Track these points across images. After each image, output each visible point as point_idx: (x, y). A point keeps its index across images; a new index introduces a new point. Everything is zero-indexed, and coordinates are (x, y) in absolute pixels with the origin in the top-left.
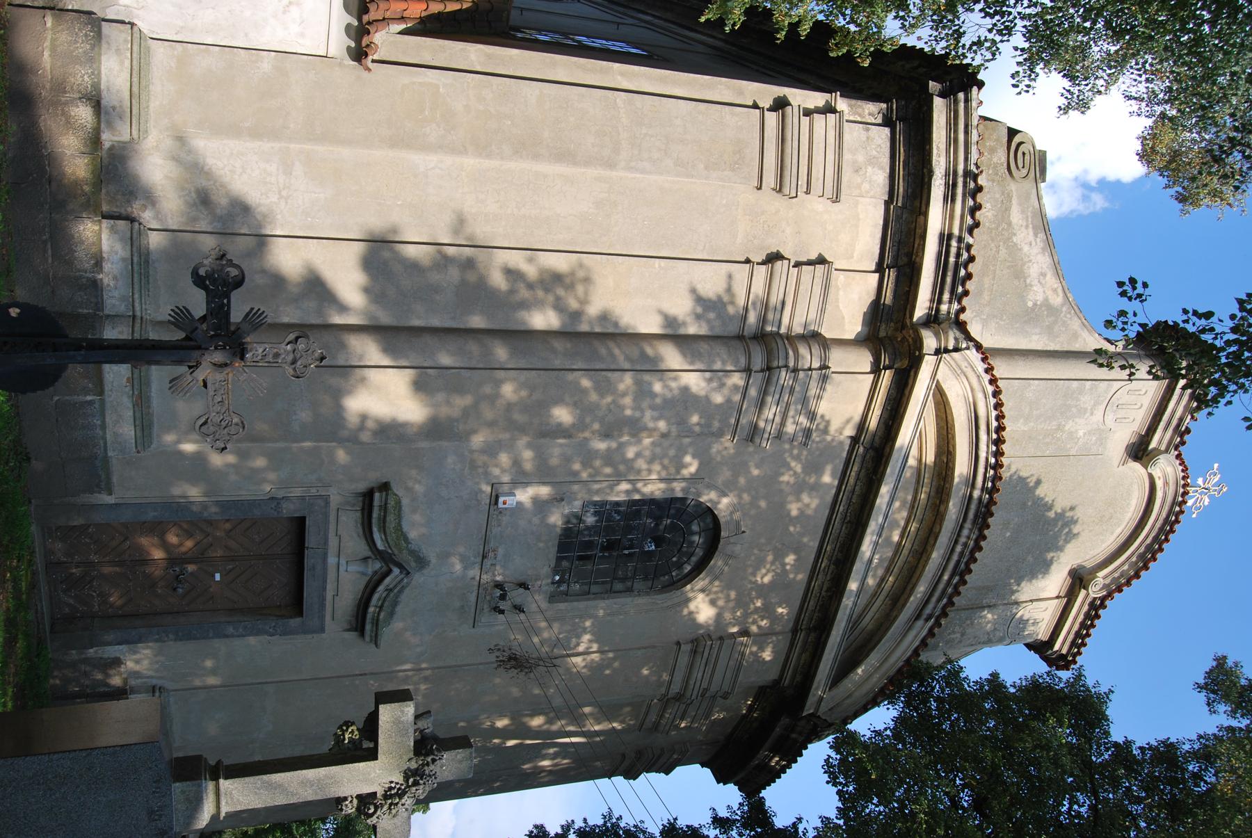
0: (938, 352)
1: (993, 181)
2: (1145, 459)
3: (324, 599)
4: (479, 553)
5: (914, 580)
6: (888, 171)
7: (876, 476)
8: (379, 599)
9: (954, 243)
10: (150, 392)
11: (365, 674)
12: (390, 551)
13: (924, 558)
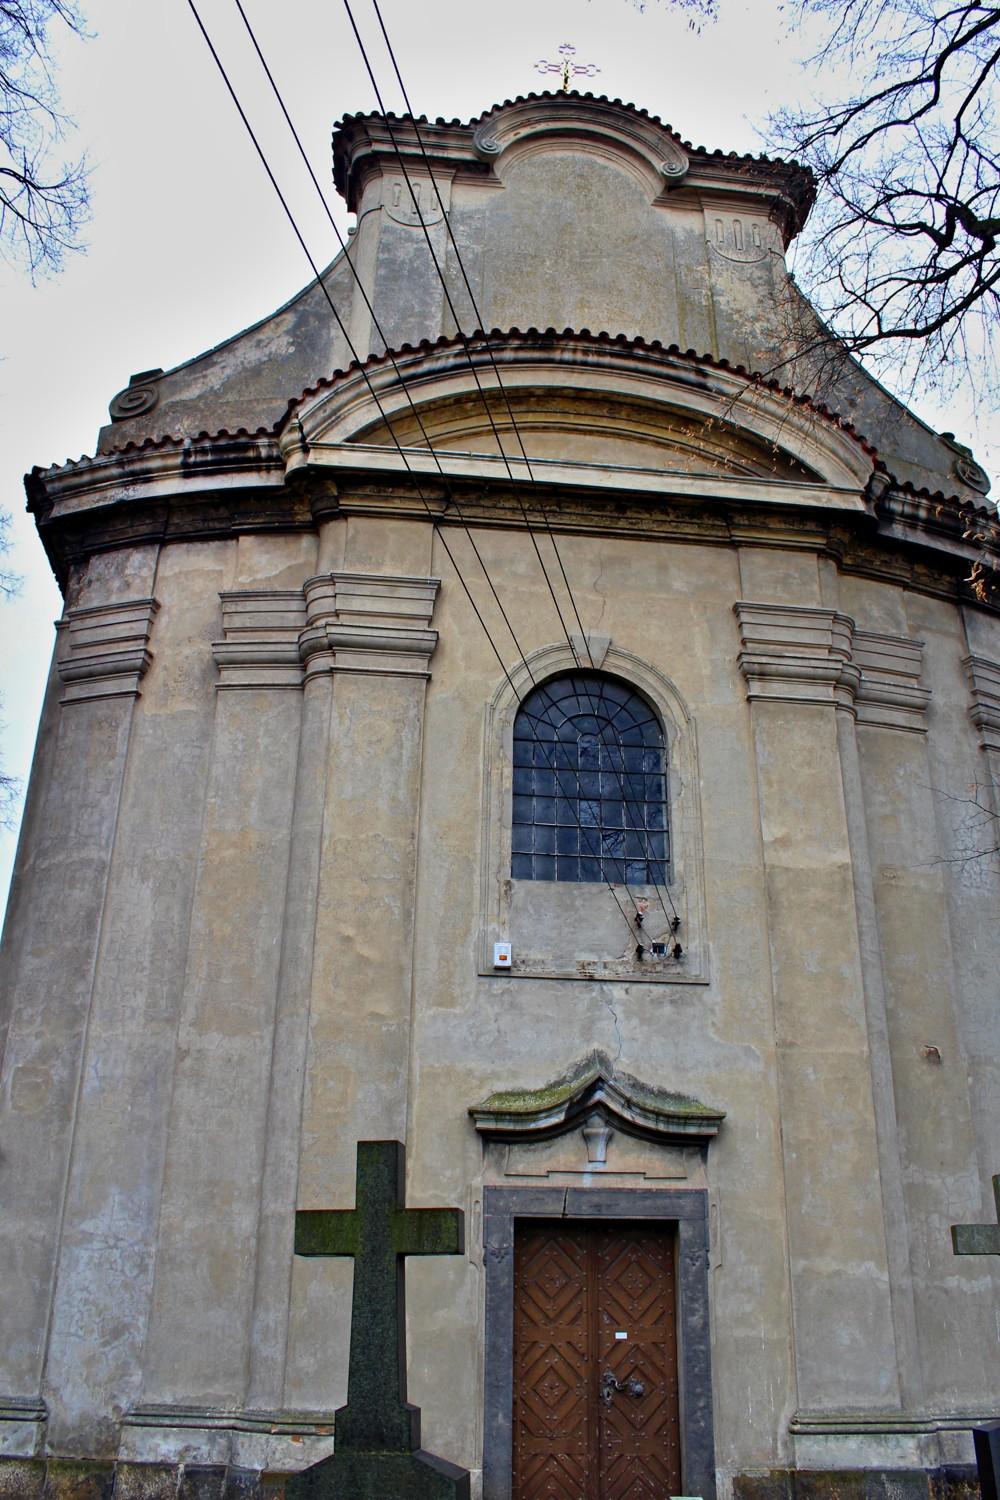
1: (153, 428)
3: (648, 1191)
4: (587, 986)
5: (650, 404)
8: (646, 1117)
10: (318, 1412)
12: (567, 1105)
13: (615, 398)
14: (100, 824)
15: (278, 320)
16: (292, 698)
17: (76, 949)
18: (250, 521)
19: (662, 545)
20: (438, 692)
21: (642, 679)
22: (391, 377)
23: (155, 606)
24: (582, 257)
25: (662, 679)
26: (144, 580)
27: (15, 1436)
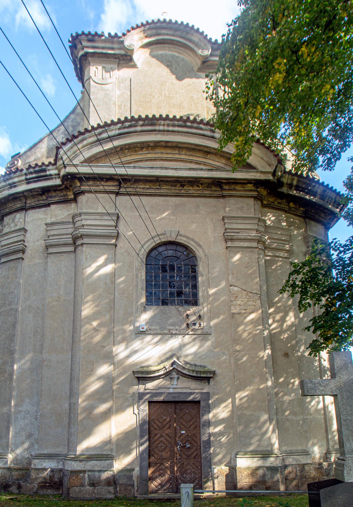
5: (193, 147)
6: (16, 214)
8: (189, 372)
9: (28, 177)
13: (180, 145)
14: (14, 298)
15: (58, 129)
16: (72, 255)
17: (10, 334)
18: (53, 199)
19: (197, 199)
20: (119, 250)
21: (189, 243)
22: (94, 139)
23: (25, 230)
24: (169, 94)
25: (196, 243)
26: (21, 223)
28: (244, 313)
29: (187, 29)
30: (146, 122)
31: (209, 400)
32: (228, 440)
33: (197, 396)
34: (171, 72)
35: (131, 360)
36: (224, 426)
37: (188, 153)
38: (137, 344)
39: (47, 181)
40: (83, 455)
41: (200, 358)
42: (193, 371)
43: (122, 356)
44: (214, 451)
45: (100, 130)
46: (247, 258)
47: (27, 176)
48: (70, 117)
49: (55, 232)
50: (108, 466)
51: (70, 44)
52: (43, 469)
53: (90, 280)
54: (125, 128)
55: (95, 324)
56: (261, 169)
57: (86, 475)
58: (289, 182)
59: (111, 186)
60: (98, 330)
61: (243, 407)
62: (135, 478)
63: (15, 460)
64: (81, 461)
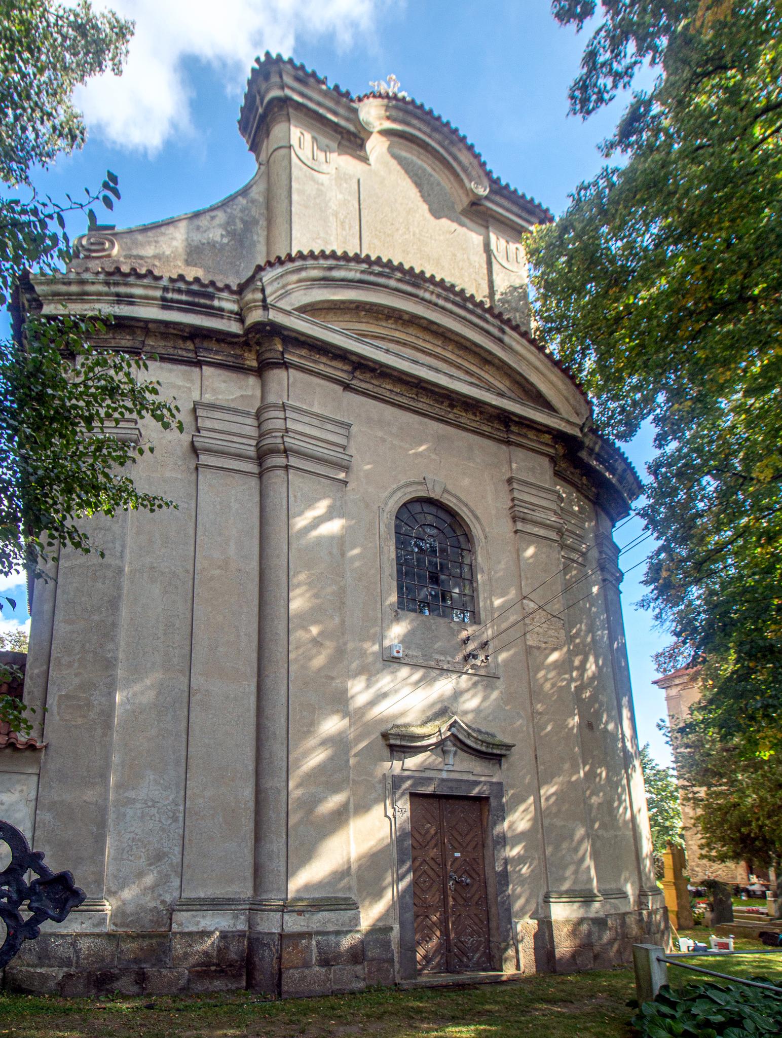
0: (265, 307)
2: (362, 135)
5: (468, 344)
7: (376, 370)
8: (476, 743)
9: (170, 295)
11: (536, 755)
13: (449, 335)
14: (113, 542)
15: (213, 214)
25: (472, 511)
27: (90, 921)
28: (545, 649)
29: (454, 137)
30: (407, 278)
31: (502, 796)
32: (532, 871)
33: (485, 788)
34: (422, 196)
35: (377, 711)
36: (524, 847)
37: (457, 352)
38: (385, 682)
39: (211, 318)
40: (301, 899)
41: (485, 719)
42: (483, 742)
43: (361, 700)
44: (514, 890)
45: (331, 262)
46: (544, 556)
47: (168, 292)
48: (236, 201)
49: (217, 425)
50: (350, 921)
51: (257, 66)
52: (202, 932)
53: (303, 542)
54: (371, 273)
55: (315, 630)
56: (565, 415)
57: (314, 943)
58: (591, 445)
59: (339, 370)
60: (321, 645)
61: (550, 813)
62: (394, 947)
63: (119, 913)
64: (300, 913)
